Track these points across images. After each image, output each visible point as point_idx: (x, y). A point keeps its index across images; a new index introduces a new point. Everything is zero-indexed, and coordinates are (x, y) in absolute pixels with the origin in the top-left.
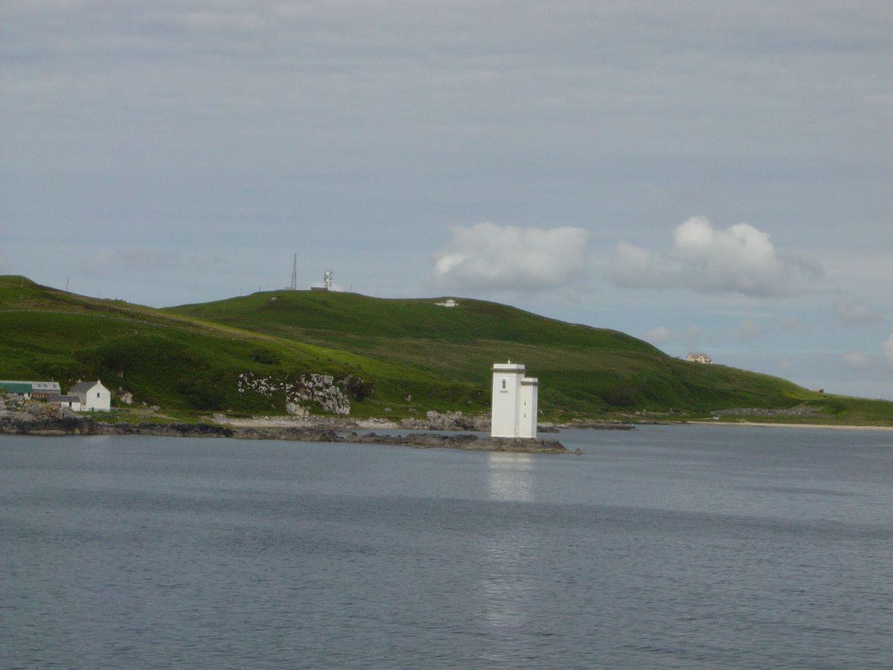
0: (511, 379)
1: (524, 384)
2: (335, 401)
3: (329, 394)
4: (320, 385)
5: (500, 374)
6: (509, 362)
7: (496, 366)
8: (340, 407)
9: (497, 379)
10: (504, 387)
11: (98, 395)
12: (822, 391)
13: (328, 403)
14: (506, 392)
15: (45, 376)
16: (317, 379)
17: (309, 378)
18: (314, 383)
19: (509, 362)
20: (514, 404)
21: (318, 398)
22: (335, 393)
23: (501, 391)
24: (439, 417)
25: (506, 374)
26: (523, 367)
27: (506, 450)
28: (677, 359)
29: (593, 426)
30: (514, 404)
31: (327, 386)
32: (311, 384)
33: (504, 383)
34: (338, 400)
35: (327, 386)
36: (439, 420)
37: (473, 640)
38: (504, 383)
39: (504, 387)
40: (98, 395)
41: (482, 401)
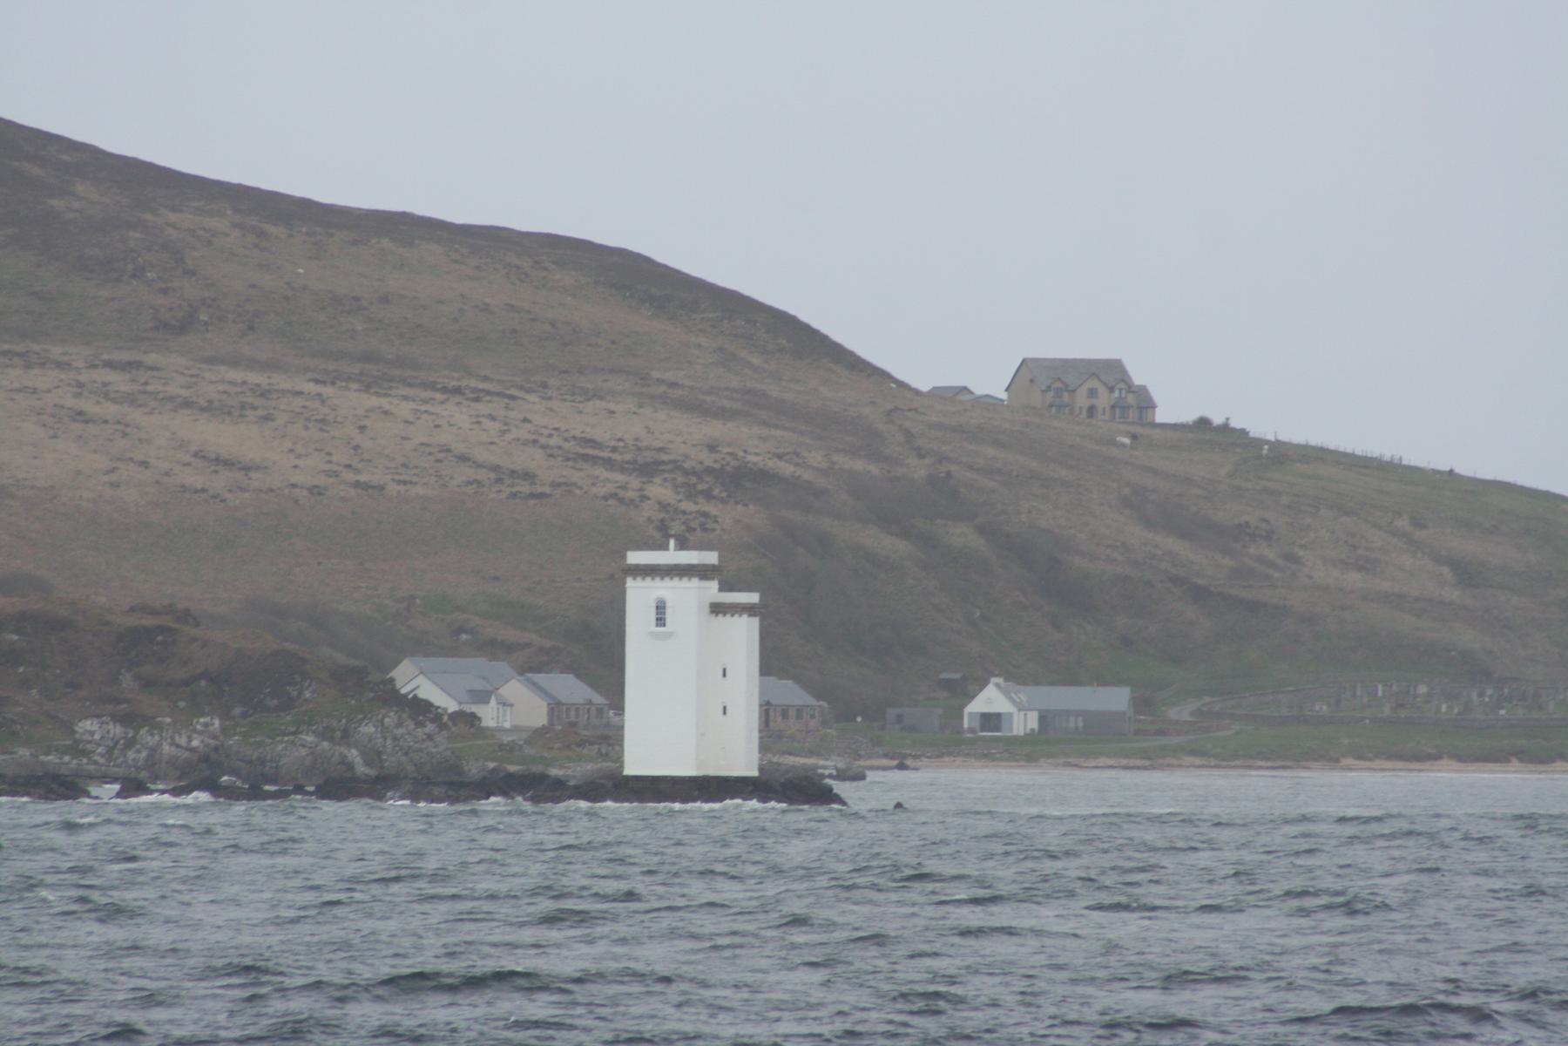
0: (688, 597)
1: (717, 609)
5: (648, 582)
6: (672, 543)
7: (635, 557)
9: (639, 596)
10: (661, 621)
12: (1451, 471)
14: (670, 635)
15: (1264, 525)
19: (672, 543)
20: (690, 680)
23: (653, 634)
24: (130, 743)
25: (667, 582)
26: (711, 558)
28: (1078, 403)
29: (724, 874)
30: (690, 680)
33: (661, 608)
36: (131, 755)
38: (661, 608)
39: (661, 621)
41: (598, 652)
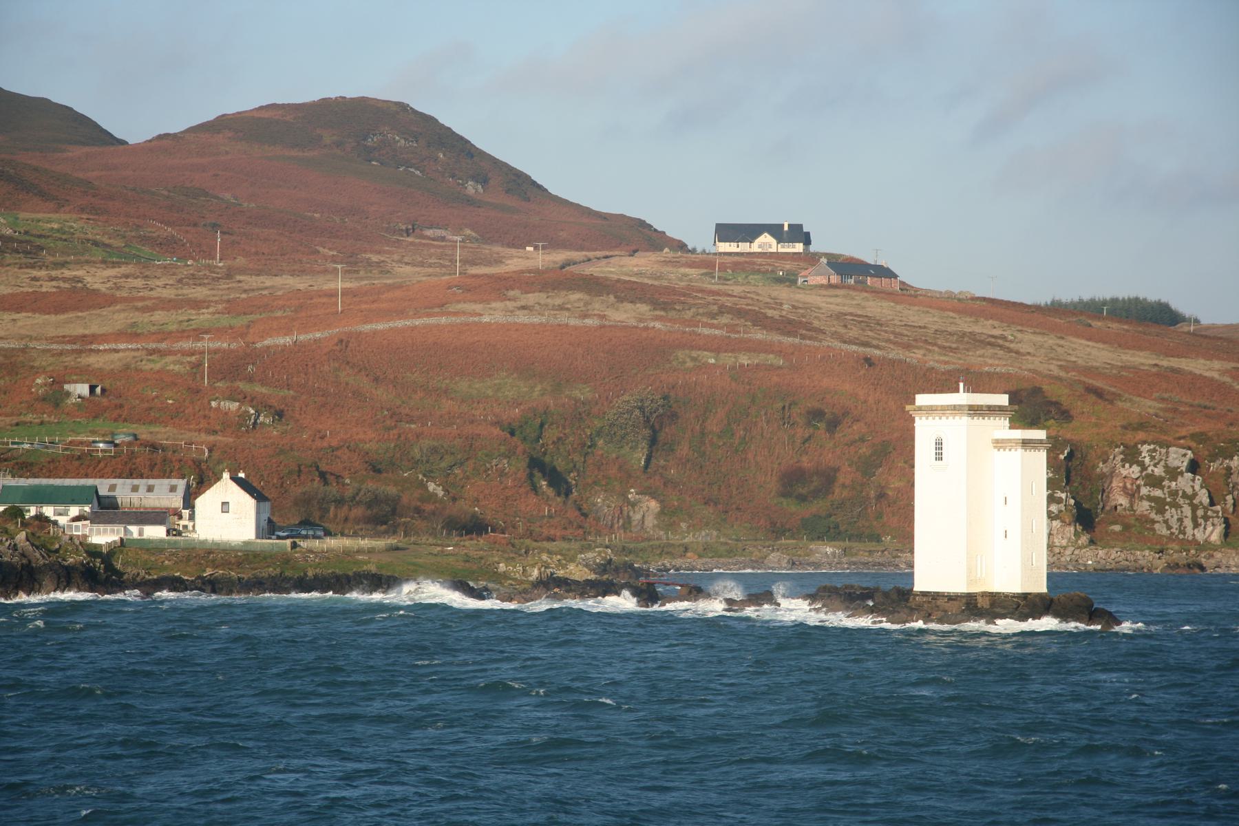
2: (1187, 511)
3: (1174, 493)
4: (1159, 471)
6: (786, 228)
7: (922, 399)
8: (1196, 525)
11: (225, 504)
13: (1168, 515)
16: (1152, 458)
17: (1131, 456)
18: (1143, 467)
19: (786, 228)
21: (1146, 504)
22: (1189, 491)
27: (141, 549)
31: (1173, 473)
32: (1136, 468)
34: (1194, 508)
35: (1173, 473)
37: (563, 657)
40: (225, 504)
